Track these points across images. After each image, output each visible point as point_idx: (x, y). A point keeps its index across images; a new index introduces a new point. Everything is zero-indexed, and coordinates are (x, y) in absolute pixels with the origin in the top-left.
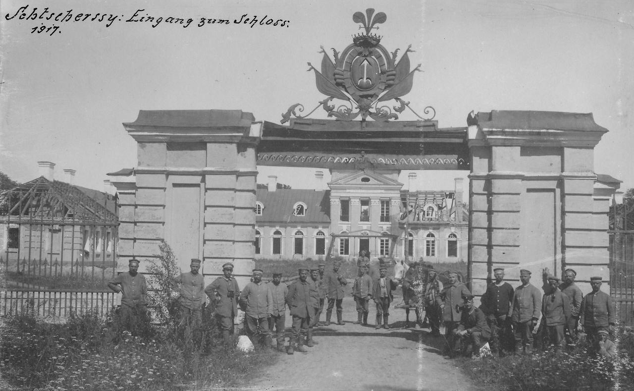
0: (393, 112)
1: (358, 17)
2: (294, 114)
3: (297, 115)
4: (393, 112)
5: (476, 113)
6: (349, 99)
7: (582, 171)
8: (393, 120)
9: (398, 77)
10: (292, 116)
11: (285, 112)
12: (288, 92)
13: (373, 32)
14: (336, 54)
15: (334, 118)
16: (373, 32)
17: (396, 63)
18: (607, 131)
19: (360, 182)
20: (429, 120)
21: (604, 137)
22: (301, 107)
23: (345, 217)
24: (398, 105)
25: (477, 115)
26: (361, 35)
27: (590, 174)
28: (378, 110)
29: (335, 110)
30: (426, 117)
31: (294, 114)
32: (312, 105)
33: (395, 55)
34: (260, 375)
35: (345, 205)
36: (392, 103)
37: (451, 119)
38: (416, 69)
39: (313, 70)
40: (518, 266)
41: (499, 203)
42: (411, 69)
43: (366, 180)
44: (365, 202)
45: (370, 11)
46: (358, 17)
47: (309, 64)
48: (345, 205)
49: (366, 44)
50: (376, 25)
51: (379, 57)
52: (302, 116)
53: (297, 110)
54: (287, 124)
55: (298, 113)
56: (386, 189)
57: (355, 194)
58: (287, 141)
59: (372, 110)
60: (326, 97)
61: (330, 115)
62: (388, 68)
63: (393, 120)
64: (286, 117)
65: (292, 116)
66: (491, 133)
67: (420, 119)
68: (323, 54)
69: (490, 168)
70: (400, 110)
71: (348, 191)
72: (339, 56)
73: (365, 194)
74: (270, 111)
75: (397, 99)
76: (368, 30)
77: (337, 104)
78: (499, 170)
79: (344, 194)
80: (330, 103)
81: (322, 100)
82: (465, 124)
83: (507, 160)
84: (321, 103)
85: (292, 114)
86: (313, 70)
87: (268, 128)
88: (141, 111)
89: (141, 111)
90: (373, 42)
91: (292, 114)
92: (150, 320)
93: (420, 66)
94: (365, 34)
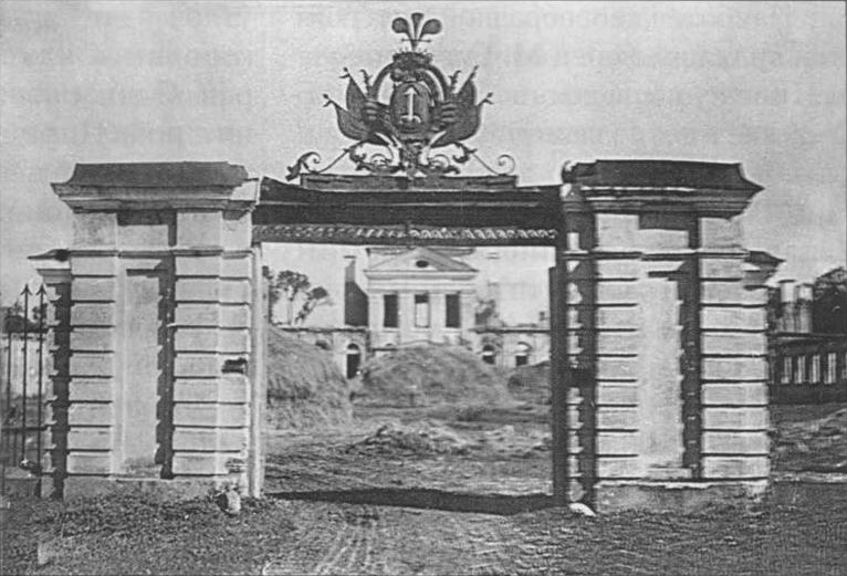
0: (453, 163)
1: (400, 26)
2: (307, 167)
3: (311, 169)
4: (453, 163)
5: (573, 163)
6: (386, 144)
7: (714, 247)
8: (452, 174)
9: (458, 113)
10: (303, 170)
11: (293, 164)
12: (303, 138)
13: (421, 47)
14: (367, 79)
15: (364, 172)
16: (421, 47)
17: (456, 91)
18: (759, 189)
19: (412, 265)
20: (504, 175)
21: (759, 196)
22: (315, 157)
23: (391, 320)
24: (460, 153)
25: (574, 168)
26: (404, 50)
27: (737, 251)
28: (431, 162)
29: (367, 160)
30: (502, 171)
31: (307, 167)
32: (334, 156)
33: (454, 79)
34: (807, 46)
35: (391, 302)
36: (453, 151)
37: (540, 170)
38: (486, 101)
39: (331, 106)
40: (654, 461)
41: (605, 293)
42: (478, 101)
43: (421, 264)
44: (422, 298)
45: (417, 17)
46: (400, 26)
47: (326, 96)
48: (391, 302)
49: (409, 66)
50: (426, 37)
51: (431, 83)
52: (318, 170)
53: (309, 161)
54: (296, 182)
55: (312, 166)
56: (454, 279)
57: (407, 288)
58: (297, 207)
59: (424, 162)
60: (354, 142)
61: (359, 168)
62: (445, 99)
63: (452, 174)
64: (294, 172)
65: (303, 170)
66: (597, 193)
67: (493, 174)
68: (347, 80)
69: (173, 241)
70: (463, 160)
71: (393, 281)
72: (372, 82)
73: (420, 286)
74: (267, 159)
75: (459, 145)
76: (414, 43)
77: (368, 150)
78: (605, 245)
79: (389, 287)
80: (359, 152)
81: (347, 147)
82: (557, 181)
83: (616, 230)
84: (346, 151)
85: (302, 166)
86: (331, 106)
87: (271, 188)
88: (78, 165)
89: (78, 165)
90: (422, 61)
91: (302, 166)
92: (158, 450)
93: (490, 95)
94: (410, 49)
